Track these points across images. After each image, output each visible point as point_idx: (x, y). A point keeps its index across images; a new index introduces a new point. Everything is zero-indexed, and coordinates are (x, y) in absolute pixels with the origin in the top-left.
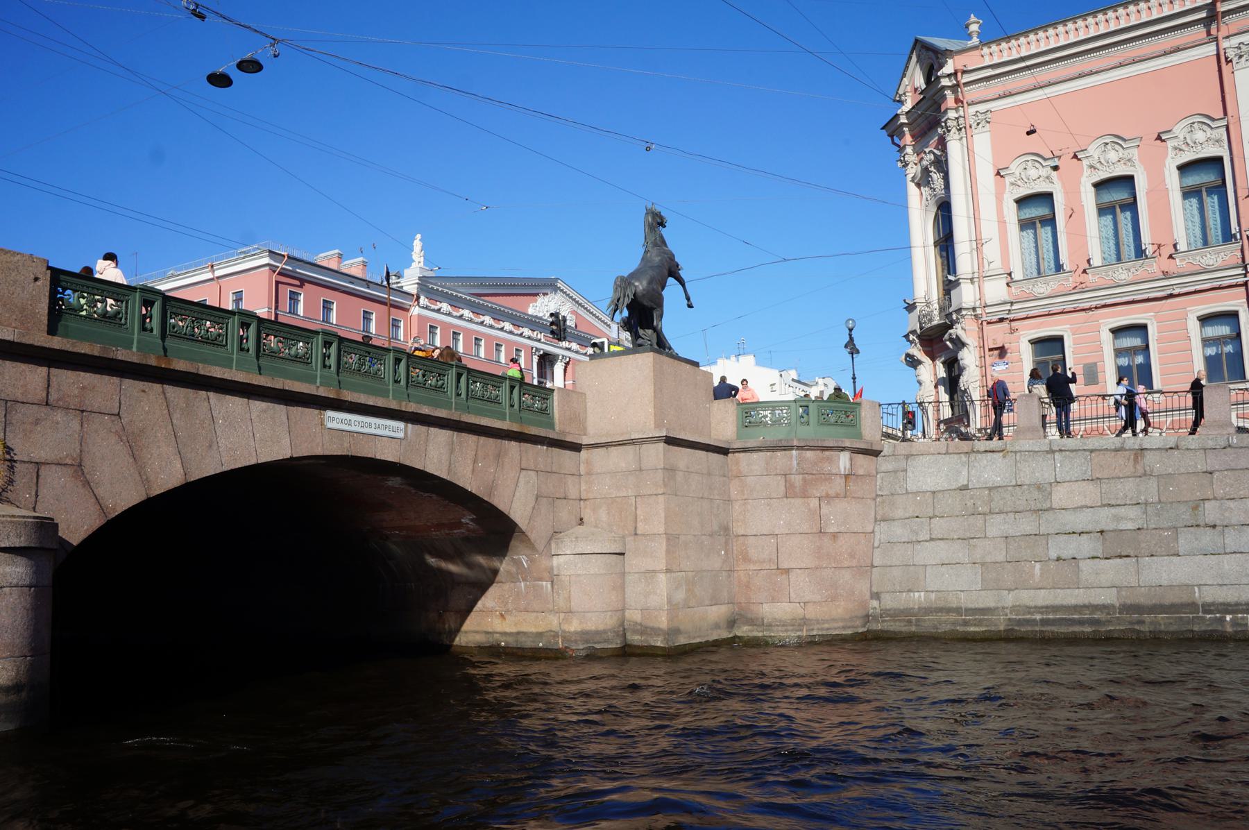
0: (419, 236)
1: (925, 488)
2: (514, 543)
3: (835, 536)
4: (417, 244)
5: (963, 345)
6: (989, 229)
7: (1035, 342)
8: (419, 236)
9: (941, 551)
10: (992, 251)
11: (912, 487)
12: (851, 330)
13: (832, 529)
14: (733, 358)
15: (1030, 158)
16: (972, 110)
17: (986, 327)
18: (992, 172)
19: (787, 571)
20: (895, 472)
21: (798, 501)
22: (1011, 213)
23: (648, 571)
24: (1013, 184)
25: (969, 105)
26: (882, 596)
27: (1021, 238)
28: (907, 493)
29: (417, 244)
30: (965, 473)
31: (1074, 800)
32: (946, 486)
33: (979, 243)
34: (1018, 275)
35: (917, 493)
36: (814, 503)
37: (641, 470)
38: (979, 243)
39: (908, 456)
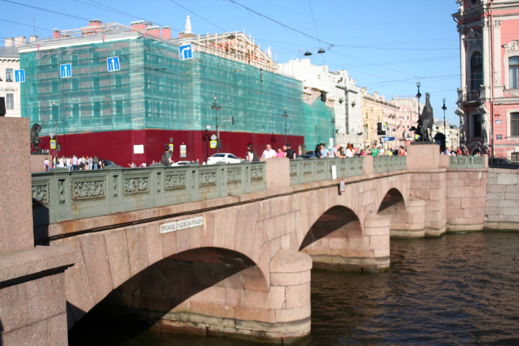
0: (188, 17)
1: (503, 183)
2: (398, 204)
3: (477, 198)
4: (188, 21)
5: (485, 112)
6: (498, 67)
7: (512, 114)
8: (188, 17)
9: (508, 203)
10: (498, 76)
11: (499, 183)
12: (419, 87)
13: (476, 196)
14: (298, 59)
15: (516, 42)
16: (494, 19)
17: (494, 107)
18: (500, 45)
19: (464, 209)
20: (493, 178)
21: (467, 188)
22: (507, 63)
23: (434, 211)
24: (508, 51)
25: (493, 16)
26: (489, 216)
27: (509, 72)
28: (497, 185)
29: (188, 21)
30: (516, 180)
31: (363, 321)
32: (510, 183)
33: (493, 73)
34: (507, 88)
35: (501, 185)
36: (472, 188)
37: (431, 181)
38: (493, 73)
39: (497, 173)
